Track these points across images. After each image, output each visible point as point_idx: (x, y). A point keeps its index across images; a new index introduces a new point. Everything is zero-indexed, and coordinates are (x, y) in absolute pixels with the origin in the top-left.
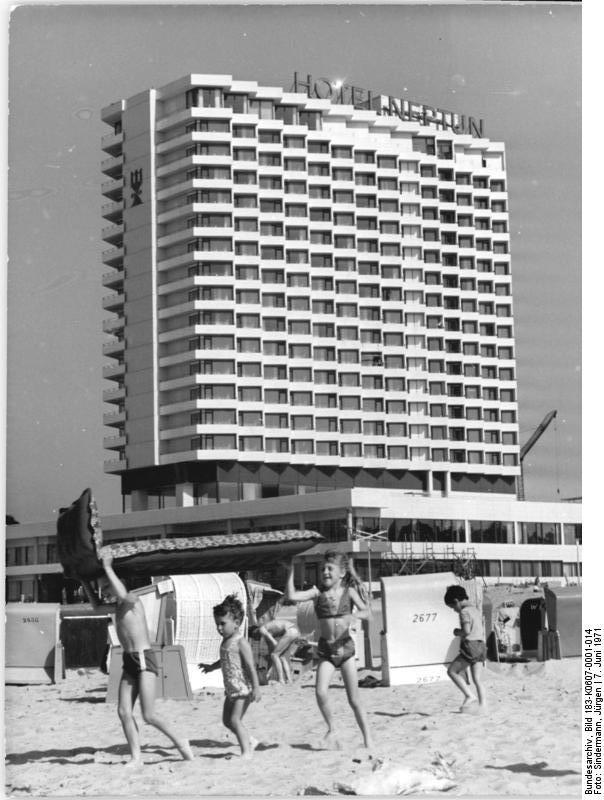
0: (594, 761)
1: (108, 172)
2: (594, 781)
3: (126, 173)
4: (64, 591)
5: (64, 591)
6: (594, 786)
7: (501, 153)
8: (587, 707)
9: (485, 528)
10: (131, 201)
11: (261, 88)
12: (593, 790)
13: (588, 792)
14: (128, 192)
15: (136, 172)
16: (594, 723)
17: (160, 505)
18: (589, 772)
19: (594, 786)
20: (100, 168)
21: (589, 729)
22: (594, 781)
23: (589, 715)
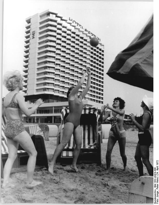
0: (156, 195)
1: (25, 52)
2: (156, 200)
3: (31, 32)
4: (92, 152)
5: (92, 152)
6: (156, 201)
7: (49, 137)
8: (155, 181)
9: (150, 131)
10: (32, 38)
11: (67, 45)
12: (156, 202)
13: (155, 203)
14: (31, 36)
15: (34, 31)
16: (156, 185)
17: (50, 53)
18: (155, 198)
19: (156, 201)
20: (23, 65)
21: (155, 187)
22: (156, 200)
23: (155, 183)
